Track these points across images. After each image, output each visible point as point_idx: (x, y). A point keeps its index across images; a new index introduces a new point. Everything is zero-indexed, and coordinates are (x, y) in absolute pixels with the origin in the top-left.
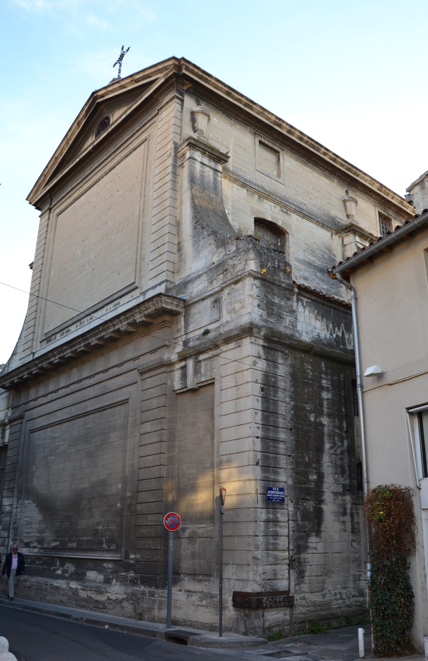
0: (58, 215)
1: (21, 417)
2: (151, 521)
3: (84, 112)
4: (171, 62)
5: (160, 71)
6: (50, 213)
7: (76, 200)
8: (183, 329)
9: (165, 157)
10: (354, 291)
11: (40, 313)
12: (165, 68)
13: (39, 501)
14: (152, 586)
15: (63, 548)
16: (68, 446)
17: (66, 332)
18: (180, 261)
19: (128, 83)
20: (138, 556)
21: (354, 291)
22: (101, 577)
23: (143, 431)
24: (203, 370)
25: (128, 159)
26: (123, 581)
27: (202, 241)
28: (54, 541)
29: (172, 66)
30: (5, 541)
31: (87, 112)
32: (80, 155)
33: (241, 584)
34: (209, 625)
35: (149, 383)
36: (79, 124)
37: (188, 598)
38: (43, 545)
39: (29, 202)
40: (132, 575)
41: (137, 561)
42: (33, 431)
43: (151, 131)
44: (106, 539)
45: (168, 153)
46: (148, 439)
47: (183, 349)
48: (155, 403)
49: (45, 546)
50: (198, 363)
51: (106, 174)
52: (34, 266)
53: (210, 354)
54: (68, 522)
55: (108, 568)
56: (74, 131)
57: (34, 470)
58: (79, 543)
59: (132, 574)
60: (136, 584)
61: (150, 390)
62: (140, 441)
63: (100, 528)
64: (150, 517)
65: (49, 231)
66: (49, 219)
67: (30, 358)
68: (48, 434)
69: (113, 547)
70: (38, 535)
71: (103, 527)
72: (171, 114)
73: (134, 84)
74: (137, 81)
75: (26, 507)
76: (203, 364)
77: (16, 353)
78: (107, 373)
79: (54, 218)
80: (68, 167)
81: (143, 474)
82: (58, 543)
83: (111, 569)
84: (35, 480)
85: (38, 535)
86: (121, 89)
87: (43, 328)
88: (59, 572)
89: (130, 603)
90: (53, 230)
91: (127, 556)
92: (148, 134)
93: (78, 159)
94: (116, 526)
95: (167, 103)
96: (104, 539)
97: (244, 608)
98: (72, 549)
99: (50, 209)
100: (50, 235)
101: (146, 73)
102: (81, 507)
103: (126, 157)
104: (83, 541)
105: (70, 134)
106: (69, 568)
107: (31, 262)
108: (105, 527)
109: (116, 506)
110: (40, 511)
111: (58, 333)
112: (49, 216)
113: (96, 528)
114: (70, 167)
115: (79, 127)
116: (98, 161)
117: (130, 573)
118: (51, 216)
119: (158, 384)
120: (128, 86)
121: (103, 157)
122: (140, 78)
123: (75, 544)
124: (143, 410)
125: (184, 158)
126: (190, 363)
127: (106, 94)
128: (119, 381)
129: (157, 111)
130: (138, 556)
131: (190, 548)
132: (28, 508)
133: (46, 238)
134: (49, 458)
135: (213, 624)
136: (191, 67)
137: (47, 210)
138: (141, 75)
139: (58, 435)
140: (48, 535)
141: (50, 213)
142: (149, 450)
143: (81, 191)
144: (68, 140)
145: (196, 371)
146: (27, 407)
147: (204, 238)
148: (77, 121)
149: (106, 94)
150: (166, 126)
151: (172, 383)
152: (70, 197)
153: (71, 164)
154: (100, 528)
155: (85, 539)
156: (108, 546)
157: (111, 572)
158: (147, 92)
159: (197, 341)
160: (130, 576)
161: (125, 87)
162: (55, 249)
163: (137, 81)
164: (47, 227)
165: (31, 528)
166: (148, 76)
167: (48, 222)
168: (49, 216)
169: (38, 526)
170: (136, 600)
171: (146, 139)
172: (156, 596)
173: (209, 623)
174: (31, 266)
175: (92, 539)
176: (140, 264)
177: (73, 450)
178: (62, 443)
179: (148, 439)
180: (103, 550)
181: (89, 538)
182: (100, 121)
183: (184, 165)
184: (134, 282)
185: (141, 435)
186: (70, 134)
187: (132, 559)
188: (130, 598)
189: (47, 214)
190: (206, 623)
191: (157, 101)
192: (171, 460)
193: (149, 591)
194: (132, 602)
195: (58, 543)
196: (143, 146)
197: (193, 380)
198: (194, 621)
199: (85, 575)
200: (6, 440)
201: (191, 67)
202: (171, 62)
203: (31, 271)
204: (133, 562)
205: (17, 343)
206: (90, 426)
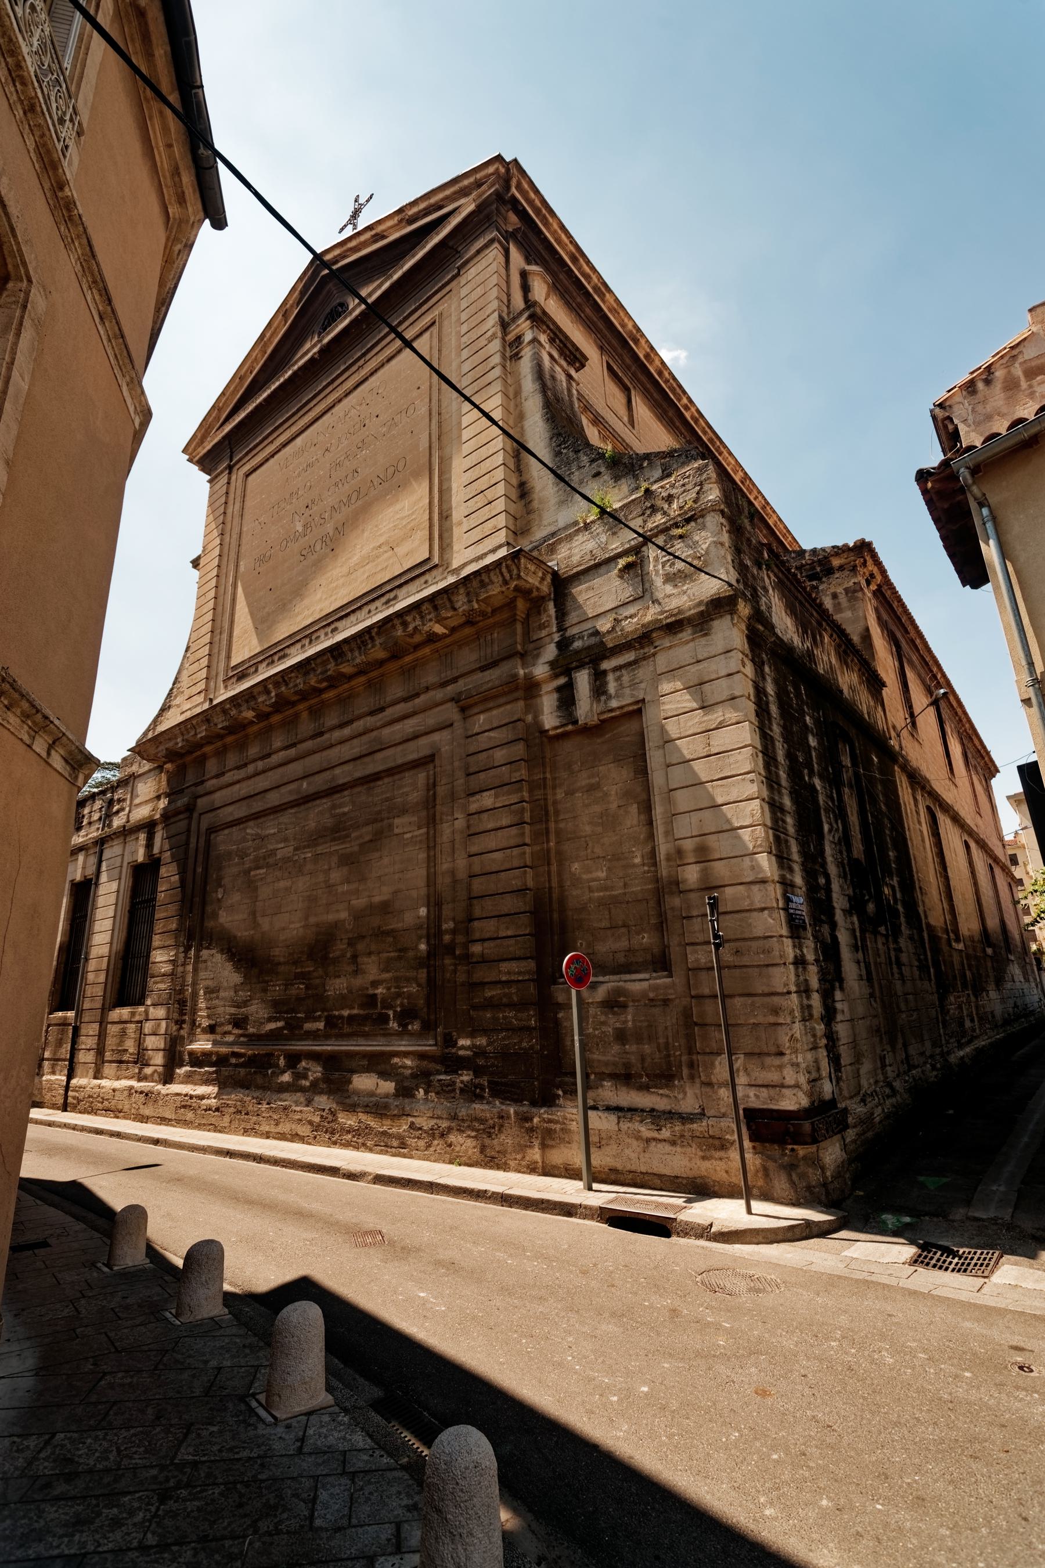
0: (247, 475)
1: (190, 809)
2: (509, 973)
3: (296, 294)
4: (491, 169)
5: (464, 192)
6: (230, 473)
7: (285, 445)
8: (554, 622)
9: (483, 341)
10: (989, 506)
11: (221, 633)
12: (478, 184)
13: (234, 950)
14: (521, 1102)
15: (293, 1030)
16: (296, 849)
17: (280, 659)
18: (528, 513)
19: (391, 227)
20: (481, 1041)
21: (989, 506)
22: (388, 1087)
23: (473, 807)
24: (612, 687)
25: (394, 362)
26: (444, 1091)
27: (577, 473)
28: (270, 1020)
29: (493, 178)
30: (159, 1025)
31: (302, 293)
32: (293, 365)
33: (764, 1093)
34: (684, 1182)
35: (481, 720)
36: (285, 316)
37: (621, 1124)
38: (246, 1029)
39: (187, 457)
40: (465, 1078)
41: (479, 1052)
42: (212, 830)
43: (441, 308)
44: (395, 1012)
45: (489, 333)
46: (488, 822)
47: (558, 656)
48: (500, 755)
49: (251, 1030)
50: (599, 678)
51: (347, 394)
52: (202, 562)
53: (630, 656)
54: (303, 983)
55: (405, 1067)
56: (276, 329)
57: (220, 896)
58: (331, 1022)
59: (466, 1077)
60: (480, 1098)
61: (486, 734)
62: (468, 827)
63: (380, 991)
64: (505, 966)
65: (231, 502)
66: (228, 483)
67: (206, 706)
68: (248, 831)
69: (415, 1026)
70: (233, 1010)
71: (389, 989)
72: (489, 269)
73: (404, 227)
74: (411, 221)
75: (205, 961)
76: (611, 678)
77: (169, 707)
78: (380, 716)
79: (240, 481)
80: (269, 388)
81: (478, 886)
82: (280, 1024)
83: (411, 1068)
84: (222, 913)
85: (233, 1010)
86: (376, 242)
87: (229, 657)
88: (286, 1077)
89: (469, 1136)
90: (238, 499)
91: (449, 1041)
92: (437, 313)
93: (290, 372)
94: (419, 985)
95: (479, 252)
96: (391, 1013)
97: (782, 1142)
98: (314, 1035)
99: (230, 468)
100: (234, 508)
101: (433, 200)
102: (331, 956)
103: (390, 359)
104: (341, 1017)
105: (268, 335)
106: (308, 1069)
107: (195, 556)
108: (393, 990)
109: (416, 948)
110: (237, 968)
111: (261, 662)
112: (229, 479)
113: (371, 992)
114: (273, 387)
115: (286, 322)
116: (328, 377)
117: (461, 1075)
118: (234, 477)
119: (504, 722)
120: (390, 234)
121: (339, 368)
122: (420, 211)
123: (323, 1024)
124: (471, 770)
125: (520, 343)
126: (583, 679)
127: (343, 256)
128: (410, 726)
129: (456, 271)
130: (481, 1041)
131: (611, 1022)
132: (209, 963)
133: (225, 513)
134: (252, 873)
135: (695, 1178)
136: (526, 186)
137: (225, 468)
138: (422, 206)
139: (272, 831)
140: (257, 1010)
141: (230, 473)
142: (491, 841)
143: (294, 429)
144: (266, 346)
145: (599, 690)
146: (200, 789)
147: (580, 468)
148: (283, 310)
149: (343, 256)
150: (479, 291)
151: (536, 717)
152: (272, 442)
153: (274, 383)
154: (380, 991)
155: (346, 1013)
156: (400, 1025)
157: (411, 1074)
158: (437, 234)
159: (593, 638)
160: (462, 1082)
161: (384, 237)
162: (245, 529)
163: (411, 221)
164: (227, 497)
165: (217, 998)
166: (439, 207)
167: (228, 489)
168: (229, 479)
169: (232, 993)
170: (484, 1130)
171: (434, 323)
172: (536, 1120)
173: (684, 1175)
174: (196, 563)
175: (362, 1012)
176: (440, 526)
177: (310, 855)
178: (282, 845)
179: (488, 822)
180: (388, 1034)
181: (355, 1011)
182: (328, 310)
183: (522, 353)
184: (429, 559)
185: (469, 815)
186: (268, 335)
187: (463, 1048)
188: (469, 1126)
189: (224, 479)
190: (677, 1177)
191: (457, 253)
192: (545, 858)
193: (516, 1112)
194: (474, 1134)
195: (280, 1024)
196: (427, 335)
197: (592, 705)
198: (641, 1173)
199: (350, 1082)
200: (156, 850)
201: (526, 186)
202: (491, 169)
203: (196, 573)
204: (469, 1053)
205: (172, 690)
206: (346, 810)
